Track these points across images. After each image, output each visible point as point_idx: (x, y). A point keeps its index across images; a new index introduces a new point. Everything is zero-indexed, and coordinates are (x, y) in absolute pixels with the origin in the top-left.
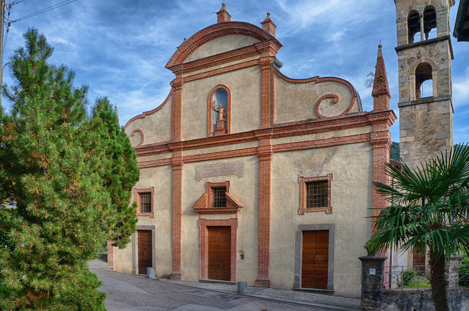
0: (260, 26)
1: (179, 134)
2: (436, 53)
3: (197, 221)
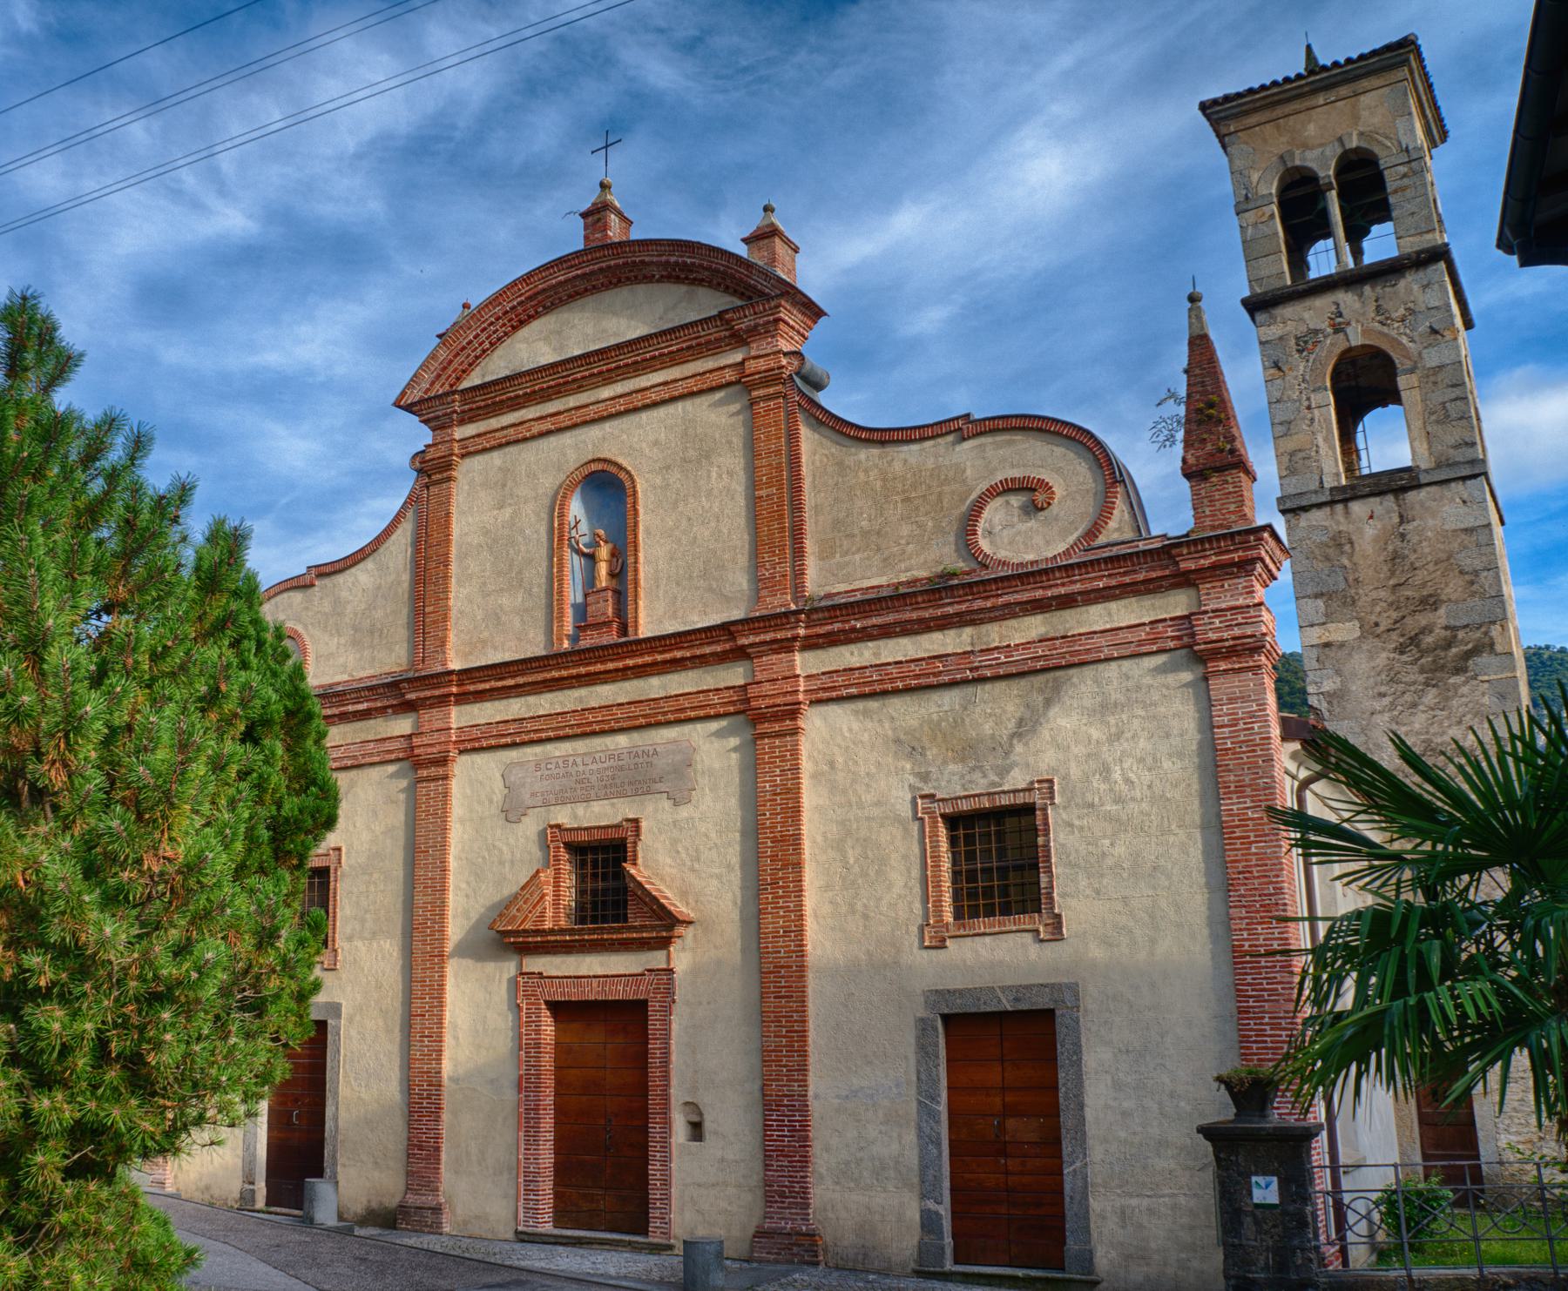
0: (742, 250)
1: (443, 642)
2: (1402, 311)
3: (509, 980)
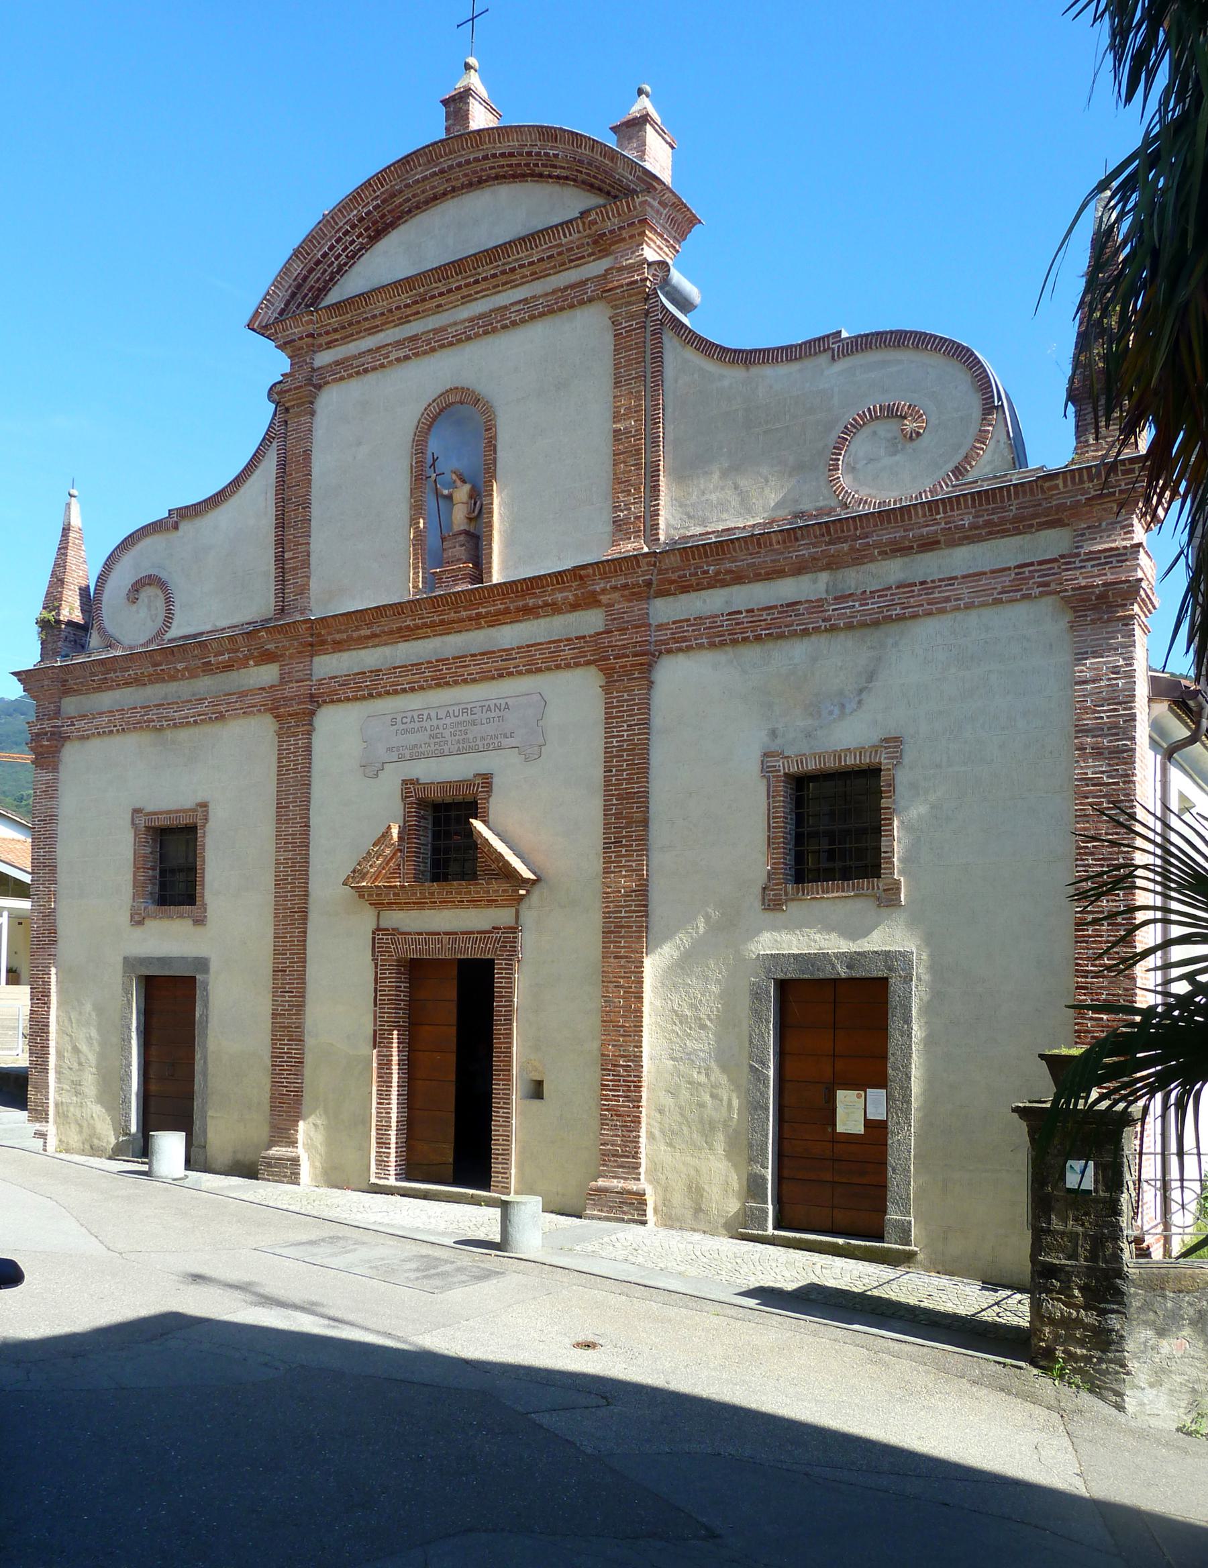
0: (611, 141)
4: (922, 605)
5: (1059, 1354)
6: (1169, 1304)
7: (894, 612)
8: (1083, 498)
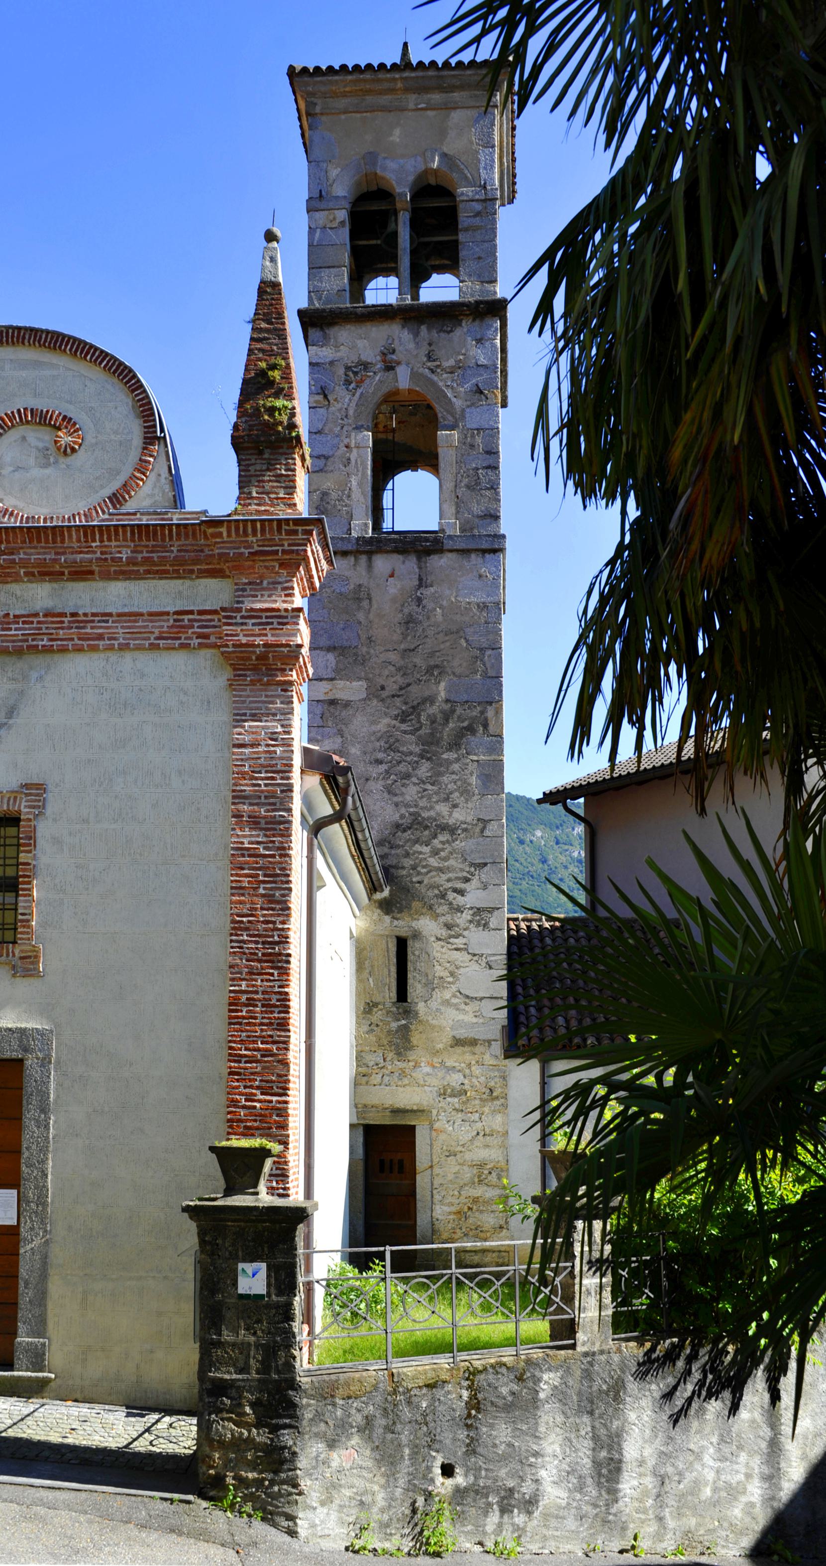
4: (72, 639)
5: (229, 1480)
6: (339, 1413)
7: (41, 643)
8: (247, 551)
